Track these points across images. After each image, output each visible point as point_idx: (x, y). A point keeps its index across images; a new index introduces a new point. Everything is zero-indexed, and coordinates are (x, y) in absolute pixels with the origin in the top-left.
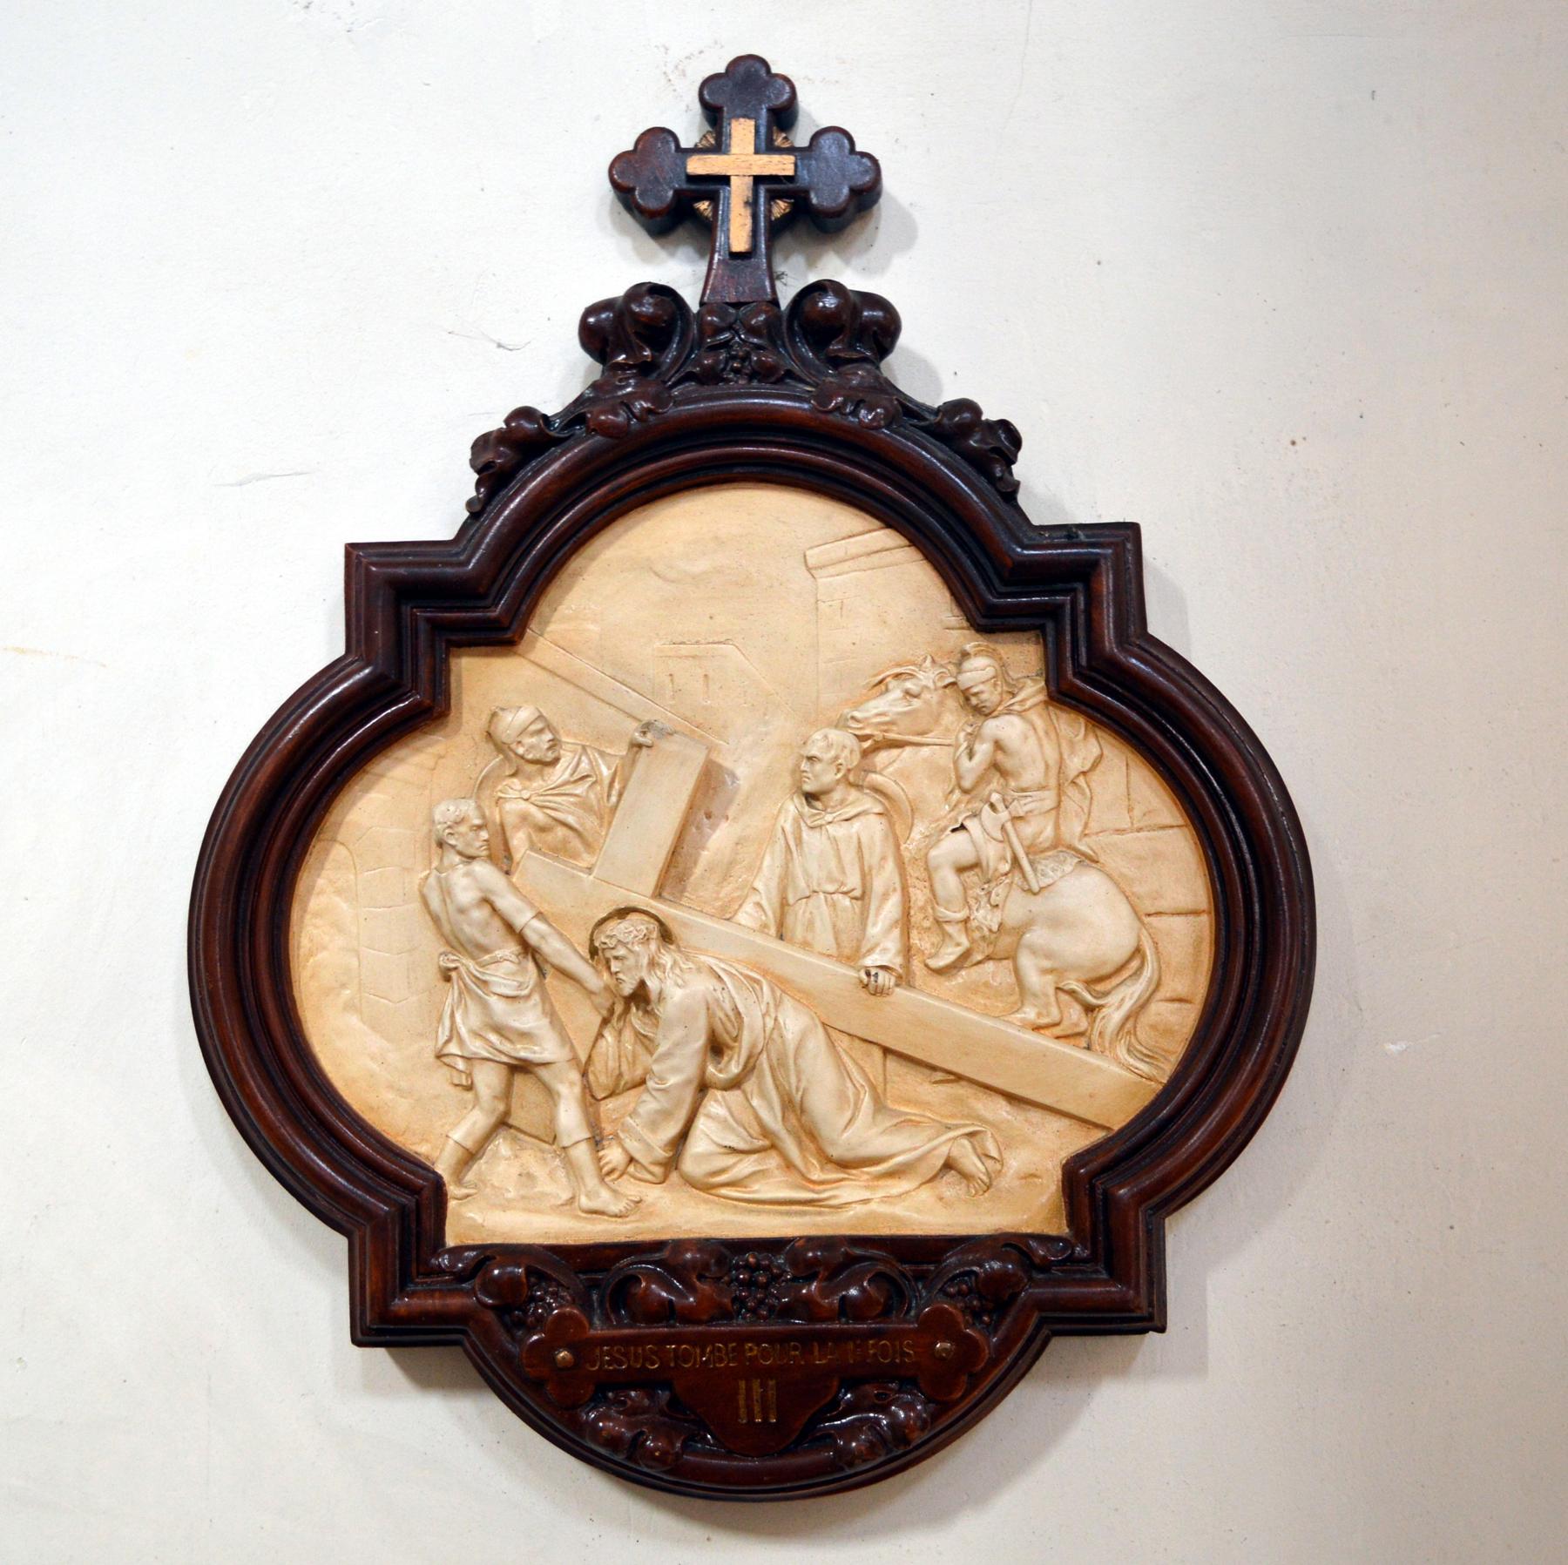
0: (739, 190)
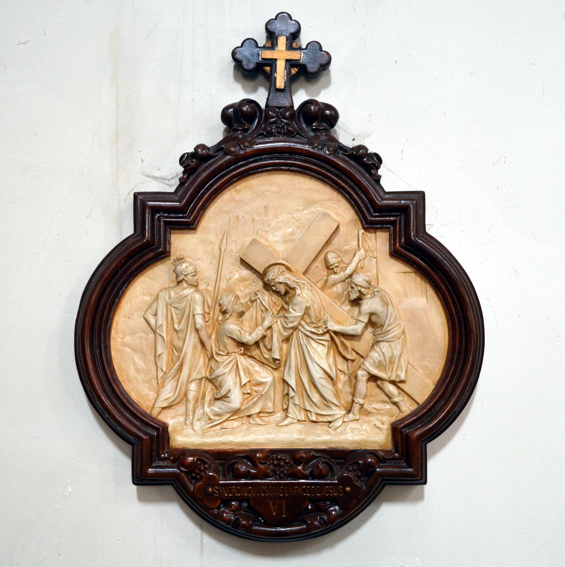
0: (281, 66)
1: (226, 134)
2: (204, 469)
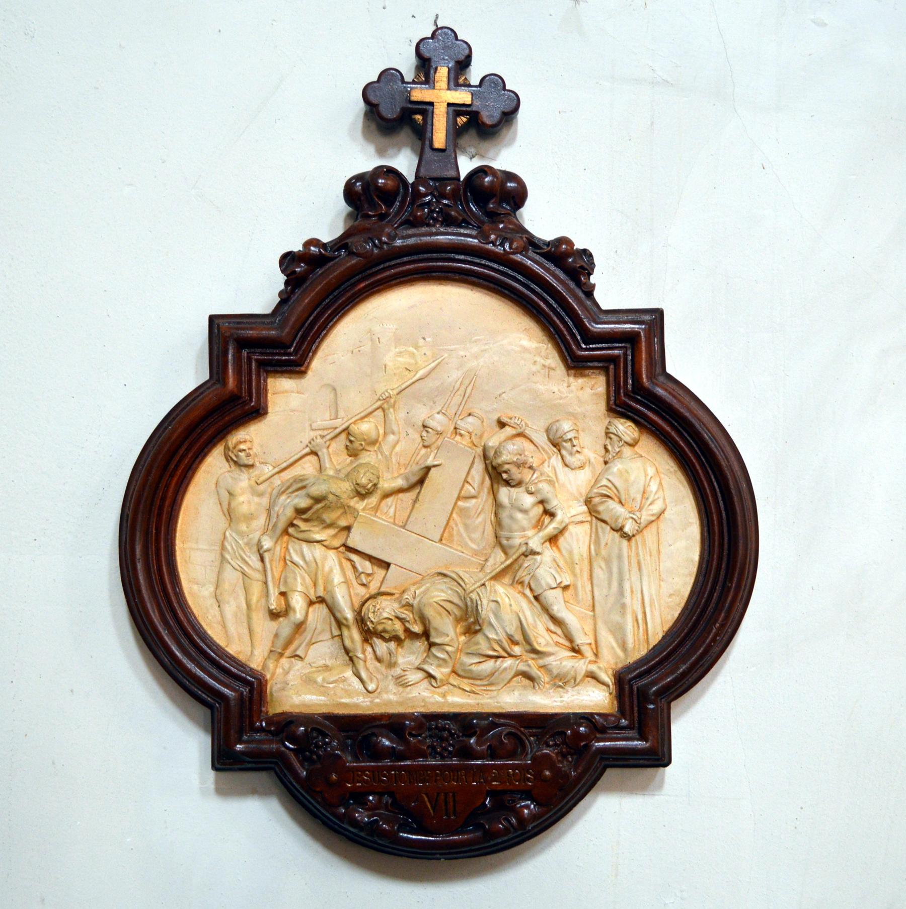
1: (351, 223)
2: (323, 745)
